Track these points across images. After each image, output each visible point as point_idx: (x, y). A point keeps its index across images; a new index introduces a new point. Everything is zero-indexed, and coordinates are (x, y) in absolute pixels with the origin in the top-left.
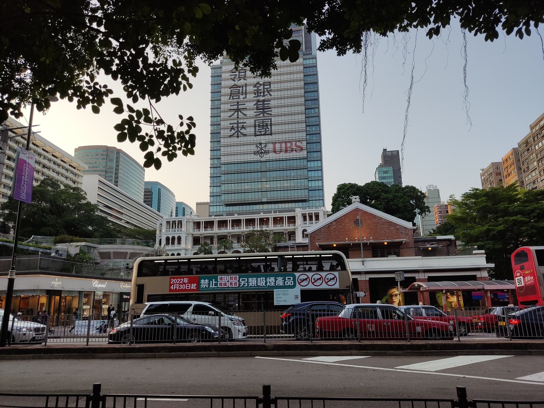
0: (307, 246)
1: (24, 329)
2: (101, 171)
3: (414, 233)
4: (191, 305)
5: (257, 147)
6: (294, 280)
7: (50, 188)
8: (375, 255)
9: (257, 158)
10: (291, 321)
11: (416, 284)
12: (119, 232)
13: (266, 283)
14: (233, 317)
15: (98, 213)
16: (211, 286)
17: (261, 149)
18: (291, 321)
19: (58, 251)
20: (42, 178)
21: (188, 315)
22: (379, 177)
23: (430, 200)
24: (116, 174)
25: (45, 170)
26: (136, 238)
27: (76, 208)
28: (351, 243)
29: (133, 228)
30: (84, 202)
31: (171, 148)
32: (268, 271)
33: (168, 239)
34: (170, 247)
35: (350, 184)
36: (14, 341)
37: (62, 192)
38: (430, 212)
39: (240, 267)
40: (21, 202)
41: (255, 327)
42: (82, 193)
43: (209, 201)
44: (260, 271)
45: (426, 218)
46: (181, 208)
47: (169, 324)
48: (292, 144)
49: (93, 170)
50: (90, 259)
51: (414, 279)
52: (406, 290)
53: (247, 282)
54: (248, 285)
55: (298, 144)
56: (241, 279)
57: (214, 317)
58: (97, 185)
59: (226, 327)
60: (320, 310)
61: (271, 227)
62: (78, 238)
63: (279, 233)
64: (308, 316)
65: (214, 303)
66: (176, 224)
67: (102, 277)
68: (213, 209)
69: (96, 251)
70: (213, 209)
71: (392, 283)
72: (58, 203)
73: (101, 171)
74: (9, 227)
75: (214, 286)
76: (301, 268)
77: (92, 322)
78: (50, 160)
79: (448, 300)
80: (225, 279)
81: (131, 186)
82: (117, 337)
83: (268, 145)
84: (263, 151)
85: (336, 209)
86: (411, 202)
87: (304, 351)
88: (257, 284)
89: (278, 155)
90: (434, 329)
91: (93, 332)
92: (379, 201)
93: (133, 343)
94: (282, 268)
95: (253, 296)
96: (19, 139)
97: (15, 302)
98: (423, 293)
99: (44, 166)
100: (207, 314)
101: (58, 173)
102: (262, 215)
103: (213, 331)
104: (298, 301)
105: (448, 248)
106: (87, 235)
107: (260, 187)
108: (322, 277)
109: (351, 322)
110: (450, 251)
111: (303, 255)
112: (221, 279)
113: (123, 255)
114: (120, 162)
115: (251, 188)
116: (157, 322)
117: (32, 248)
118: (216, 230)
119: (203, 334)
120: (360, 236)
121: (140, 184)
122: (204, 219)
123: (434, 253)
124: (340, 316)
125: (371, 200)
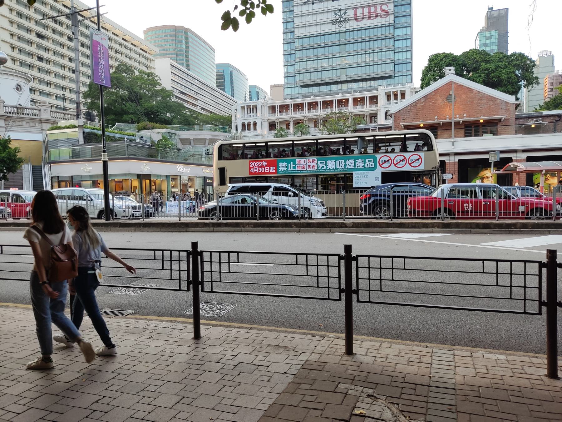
0: (391, 127)
1: (123, 207)
2: (172, 54)
3: (516, 108)
4: (270, 187)
5: (336, 14)
6: (375, 162)
7: (124, 74)
8: (468, 134)
9: (335, 28)
10: (370, 201)
11: (512, 165)
12: (196, 118)
13: (345, 165)
14: (312, 198)
15: (174, 99)
16: (289, 170)
17: (340, 17)
18: (370, 201)
19: (142, 137)
20: (116, 64)
21: (269, 195)
22: (480, 45)
23: (541, 70)
24: (187, 56)
25: (118, 56)
26: (212, 124)
27: (153, 94)
28: (441, 122)
29: (208, 114)
30: (159, 88)
31: (248, 6)
32: (347, 153)
33: (243, 125)
34: (246, 133)
35: (444, 53)
36: (116, 216)
37: (138, 78)
38: (539, 83)
39: (318, 149)
40: (101, 86)
41: (334, 208)
42: (157, 78)
43: (283, 83)
44: (340, 154)
45: (534, 92)
46: (255, 92)
47: (252, 203)
48: (376, 9)
49: (164, 54)
50: (172, 145)
51: (510, 160)
52: (501, 171)
53: (326, 165)
54: (327, 167)
55: (384, 7)
56: (319, 162)
57: (294, 198)
58: (169, 69)
59: (305, 208)
60: (402, 192)
61: (351, 109)
62: (158, 125)
63: (359, 115)
64: (389, 197)
65: (293, 185)
66: (250, 109)
67: (185, 162)
68: (288, 92)
69: (177, 137)
70: (288, 92)
71: (485, 164)
72: (136, 90)
73: (172, 54)
74: (94, 115)
75: (292, 169)
76: (383, 150)
77: (182, 202)
78: (121, 45)
79: (547, 182)
80: (303, 162)
81: (202, 69)
82: (206, 214)
83: (348, 11)
84: (342, 19)
85: (425, 83)
86: (517, 72)
87: (383, 229)
88: (335, 167)
89: (359, 23)
90: (537, 208)
91: (184, 212)
92: (478, 73)
93: (220, 219)
94: (363, 150)
95: (332, 179)
96: (87, 22)
97: (112, 185)
98: (519, 175)
99: (116, 52)
100: (287, 195)
101: (131, 58)
102: (341, 96)
103: (293, 210)
104: (379, 183)
105: (555, 125)
106: (166, 122)
107: (338, 63)
108: (405, 158)
109: (446, 202)
110: (557, 128)
111: (386, 135)
112: (299, 162)
113: (202, 141)
114: (189, 43)
115: (329, 65)
116: (240, 202)
117: (117, 135)
118: (292, 115)
119: (283, 213)
120: (453, 114)
121: (211, 71)
122: (278, 103)
123: (538, 130)
124: (435, 195)
125: (469, 72)
